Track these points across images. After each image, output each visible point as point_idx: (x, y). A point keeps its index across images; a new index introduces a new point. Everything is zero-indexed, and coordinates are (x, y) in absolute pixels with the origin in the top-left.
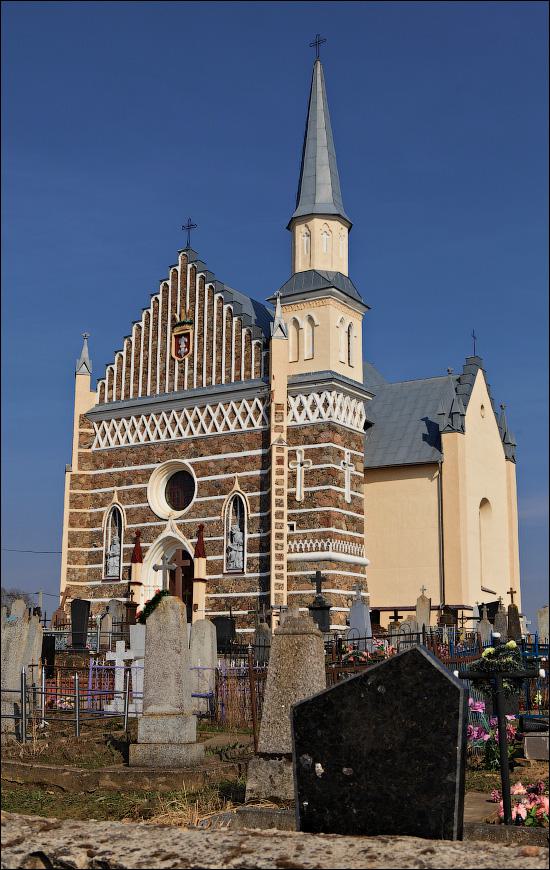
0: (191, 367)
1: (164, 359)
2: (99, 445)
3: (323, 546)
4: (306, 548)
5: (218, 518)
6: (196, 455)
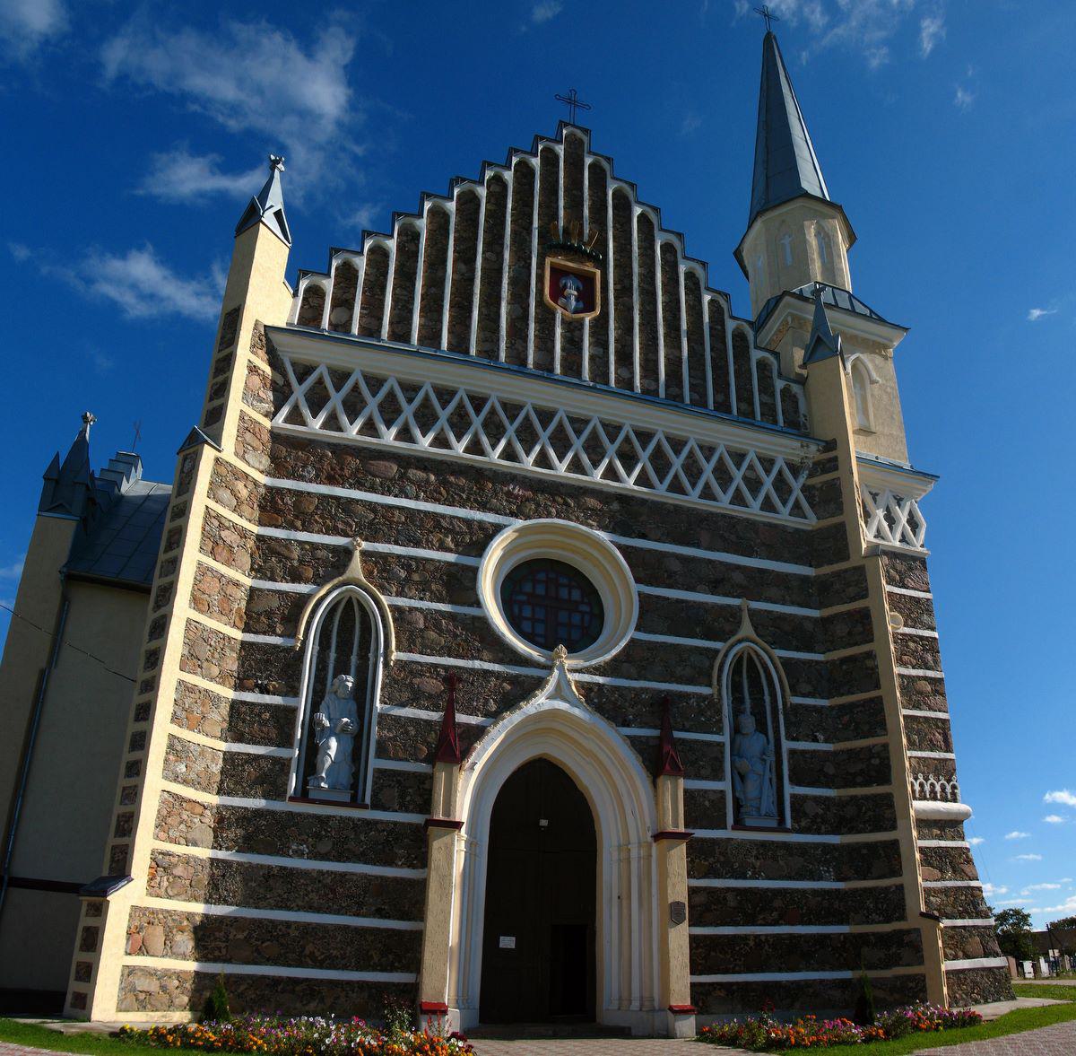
4: (933, 791)
5: (705, 691)
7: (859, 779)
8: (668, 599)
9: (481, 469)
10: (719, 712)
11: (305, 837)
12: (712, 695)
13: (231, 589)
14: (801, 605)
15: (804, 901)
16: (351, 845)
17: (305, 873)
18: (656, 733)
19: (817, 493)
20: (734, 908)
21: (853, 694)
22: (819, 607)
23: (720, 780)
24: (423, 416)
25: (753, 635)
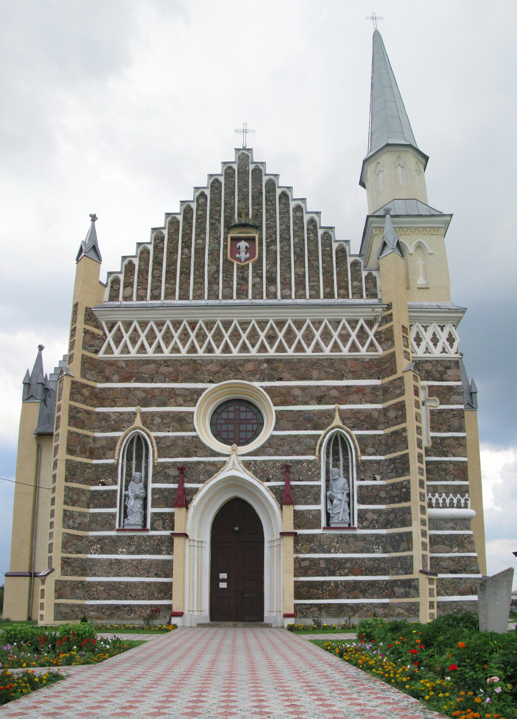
0: (258, 275)
1: (214, 260)
2: (109, 350)
3: (459, 501)
4: (437, 503)
5: (312, 458)
6: (272, 379)
7: (396, 499)
8: (293, 411)
9: (196, 360)
10: (320, 468)
11: (124, 545)
12: (315, 460)
13: (85, 439)
14: (371, 402)
15: (363, 564)
16: (143, 547)
17: (125, 561)
18: (283, 483)
19: (383, 336)
20: (324, 568)
21: (396, 452)
22: (384, 401)
23: (318, 504)
24: (167, 338)
25: (340, 424)
